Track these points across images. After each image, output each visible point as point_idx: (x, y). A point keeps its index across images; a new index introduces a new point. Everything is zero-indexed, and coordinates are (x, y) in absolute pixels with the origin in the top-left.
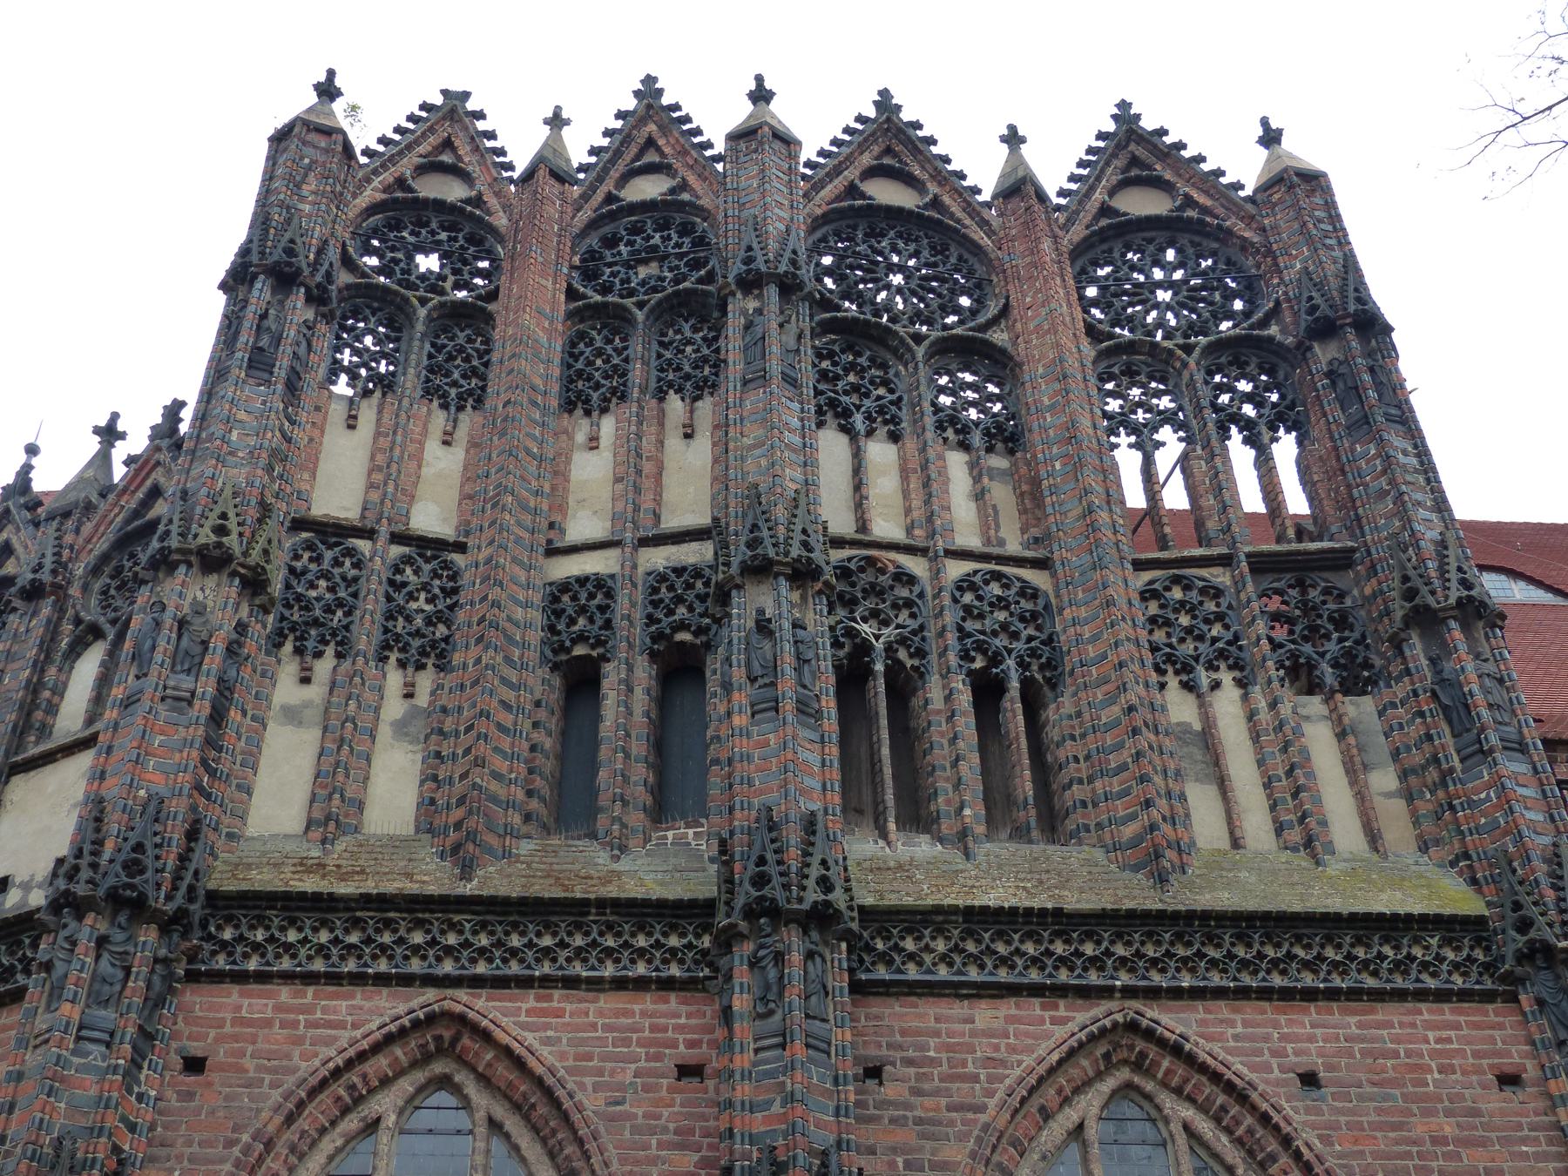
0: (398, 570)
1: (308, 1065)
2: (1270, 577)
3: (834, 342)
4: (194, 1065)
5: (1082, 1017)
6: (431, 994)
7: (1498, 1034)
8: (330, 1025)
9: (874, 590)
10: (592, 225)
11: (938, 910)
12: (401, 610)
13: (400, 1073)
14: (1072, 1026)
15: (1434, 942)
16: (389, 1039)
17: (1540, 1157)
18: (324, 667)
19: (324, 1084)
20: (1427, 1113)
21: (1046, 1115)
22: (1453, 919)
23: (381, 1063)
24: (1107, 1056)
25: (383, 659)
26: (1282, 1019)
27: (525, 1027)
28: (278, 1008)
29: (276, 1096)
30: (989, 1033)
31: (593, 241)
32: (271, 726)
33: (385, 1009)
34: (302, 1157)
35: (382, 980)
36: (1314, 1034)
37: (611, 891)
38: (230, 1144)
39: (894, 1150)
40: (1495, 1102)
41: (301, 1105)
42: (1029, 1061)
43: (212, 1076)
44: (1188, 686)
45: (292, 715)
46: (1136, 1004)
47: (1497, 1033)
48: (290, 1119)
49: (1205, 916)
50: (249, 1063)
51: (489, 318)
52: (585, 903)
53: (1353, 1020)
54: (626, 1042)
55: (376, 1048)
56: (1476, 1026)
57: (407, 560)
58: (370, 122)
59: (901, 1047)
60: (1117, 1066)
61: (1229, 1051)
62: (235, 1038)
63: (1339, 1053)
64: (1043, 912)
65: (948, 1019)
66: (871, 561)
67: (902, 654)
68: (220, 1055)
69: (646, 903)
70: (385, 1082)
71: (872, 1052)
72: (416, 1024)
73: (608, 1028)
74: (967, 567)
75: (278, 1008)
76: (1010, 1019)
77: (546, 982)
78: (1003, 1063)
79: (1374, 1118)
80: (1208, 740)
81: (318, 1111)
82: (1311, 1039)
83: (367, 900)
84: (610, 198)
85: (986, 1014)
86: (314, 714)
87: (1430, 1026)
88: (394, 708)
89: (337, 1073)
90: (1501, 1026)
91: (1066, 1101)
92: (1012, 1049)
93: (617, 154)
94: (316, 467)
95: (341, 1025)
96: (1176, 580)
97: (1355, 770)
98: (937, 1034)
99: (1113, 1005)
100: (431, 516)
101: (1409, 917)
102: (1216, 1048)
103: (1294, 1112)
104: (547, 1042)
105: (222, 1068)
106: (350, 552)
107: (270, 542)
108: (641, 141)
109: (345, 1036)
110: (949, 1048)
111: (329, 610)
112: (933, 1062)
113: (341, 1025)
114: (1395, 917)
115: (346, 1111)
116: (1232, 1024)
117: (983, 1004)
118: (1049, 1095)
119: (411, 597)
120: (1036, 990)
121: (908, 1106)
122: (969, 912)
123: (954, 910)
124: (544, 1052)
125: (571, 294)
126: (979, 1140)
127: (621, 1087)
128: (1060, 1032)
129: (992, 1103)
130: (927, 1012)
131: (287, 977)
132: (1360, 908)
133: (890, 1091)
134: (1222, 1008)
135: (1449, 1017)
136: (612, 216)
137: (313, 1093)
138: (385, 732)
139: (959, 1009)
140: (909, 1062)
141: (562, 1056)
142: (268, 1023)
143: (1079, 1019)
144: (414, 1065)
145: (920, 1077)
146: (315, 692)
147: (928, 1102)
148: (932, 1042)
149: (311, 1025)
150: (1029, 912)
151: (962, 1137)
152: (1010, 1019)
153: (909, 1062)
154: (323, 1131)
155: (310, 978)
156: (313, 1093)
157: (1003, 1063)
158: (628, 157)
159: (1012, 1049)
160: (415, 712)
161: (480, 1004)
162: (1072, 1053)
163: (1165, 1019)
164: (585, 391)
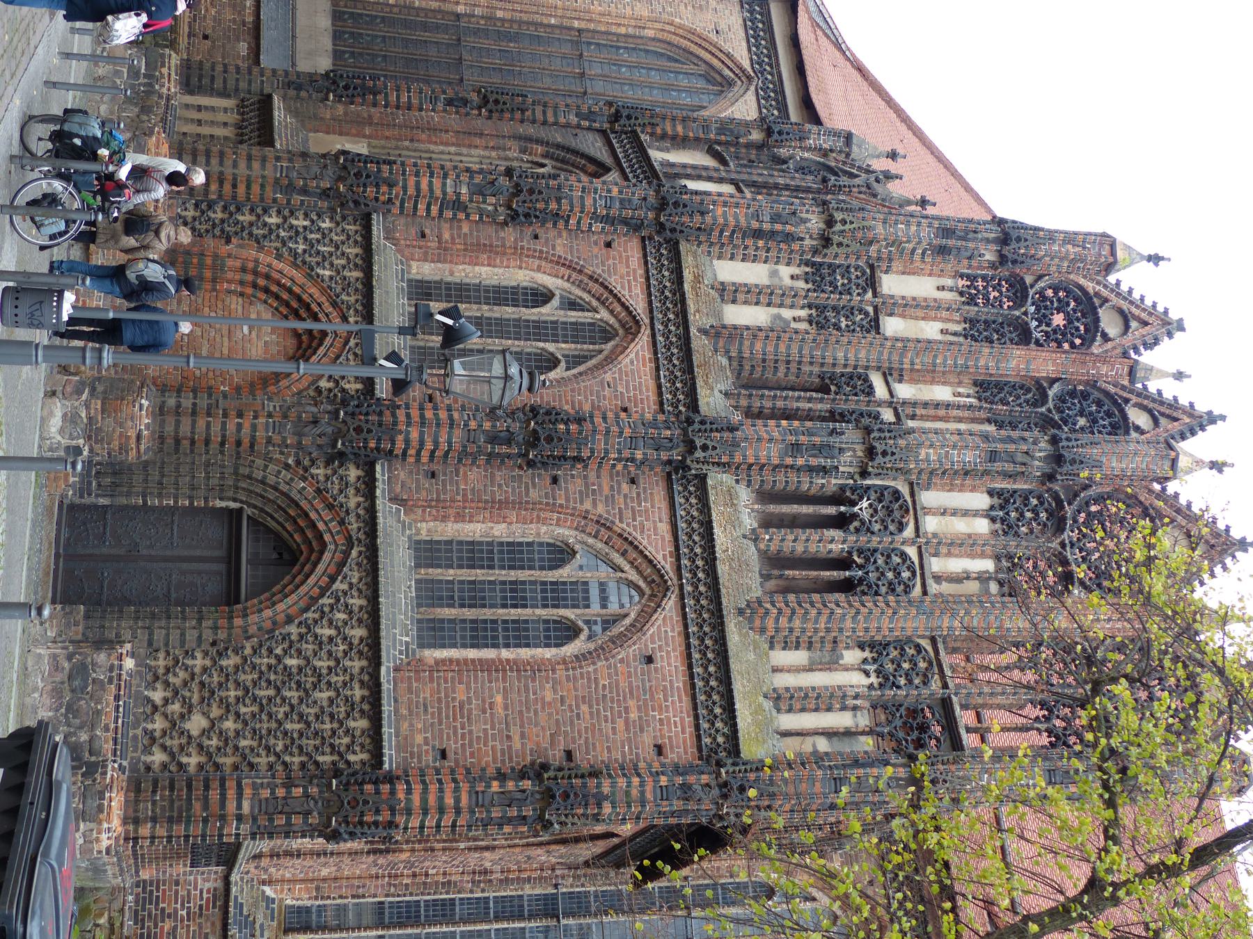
0: (860, 311)
1: (614, 282)
2: (942, 712)
3: (1050, 504)
4: (608, 245)
5: (668, 567)
6: (647, 321)
7: (682, 748)
8: (630, 288)
9: (890, 512)
10: (1107, 393)
11: (709, 509)
12: (838, 313)
13: (616, 317)
14: (663, 563)
15: (725, 730)
16: (627, 308)
17: (623, 753)
18: (801, 284)
19: (606, 288)
20: (639, 708)
21: (624, 554)
22: (737, 738)
23: (619, 309)
24: (653, 581)
25: (810, 307)
26: (678, 653)
27: (637, 353)
28: (634, 270)
29: (599, 271)
30: (655, 528)
31: (1096, 394)
32: (767, 266)
33: (639, 304)
34: (579, 286)
35: (650, 303)
36: (671, 664)
37: (700, 383)
38: (579, 258)
39: (600, 486)
40: (647, 740)
41: (596, 281)
42: (645, 542)
43: (604, 251)
44: (865, 661)
45: (774, 274)
46: (677, 591)
47: (682, 750)
48: (591, 278)
49: (722, 624)
50: (611, 262)
51: (1028, 344)
52: (693, 372)
53: (681, 685)
54: (635, 389)
55: (623, 305)
56: (685, 741)
57: (866, 314)
58: (1133, 279)
59: (645, 492)
60: (652, 589)
61: (659, 627)
62: (620, 257)
63: (664, 675)
64: (714, 552)
65: (660, 513)
66: (907, 511)
67: (856, 524)
68: (612, 253)
69: (696, 394)
70: (612, 312)
71: (641, 481)
72: (634, 317)
73: (640, 383)
74: (915, 559)
75: (634, 270)
76: (663, 538)
77: (657, 359)
78: (642, 532)
79: (634, 684)
80: (832, 664)
81: (596, 288)
82: (669, 665)
83: (683, 295)
84: (1127, 401)
85: (664, 528)
86: (776, 281)
87: (682, 719)
88: (787, 314)
89: (611, 292)
90: (686, 753)
91: (631, 563)
92: (649, 536)
93: (1162, 403)
94: (909, 274)
95: (630, 291)
96: (930, 663)
97: (830, 734)
98: (653, 507)
99: (675, 581)
100: (892, 326)
101: (734, 717)
102: (660, 622)
103: (632, 650)
104: (632, 362)
105: (608, 254)
106: (865, 291)
107: (848, 246)
108: (1175, 414)
109: (626, 293)
110: (647, 511)
111: (831, 283)
112: (640, 505)
113: (630, 291)
114: (734, 711)
115: (598, 299)
116: (673, 631)
117: (669, 527)
118: (633, 554)
119: (847, 317)
120: (677, 548)
121: (619, 492)
122: (710, 522)
123: (710, 516)
124: (627, 360)
125: (1053, 381)
126: (607, 519)
127: (615, 386)
128: (660, 558)
129: (624, 526)
130: (661, 503)
131: (647, 271)
132: (736, 694)
133: (625, 487)
134: (679, 628)
135: (690, 751)
136: (1115, 402)
137: (602, 284)
138: (775, 311)
139: (665, 516)
140: (638, 494)
141: (626, 366)
142: (628, 267)
143: (667, 566)
144: (620, 321)
145: (632, 499)
146: (787, 282)
147: (622, 500)
148: (649, 505)
149: (629, 281)
150: (714, 546)
151: (608, 512)
152: (663, 538)
153: (638, 494)
154: (589, 292)
155: (648, 279)
156: (602, 284)
157: (642, 532)
158: (1162, 409)
159: (649, 536)
160: (787, 323)
161: (645, 338)
162: (650, 562)
163: (671, 602)
164: (988, 388)
